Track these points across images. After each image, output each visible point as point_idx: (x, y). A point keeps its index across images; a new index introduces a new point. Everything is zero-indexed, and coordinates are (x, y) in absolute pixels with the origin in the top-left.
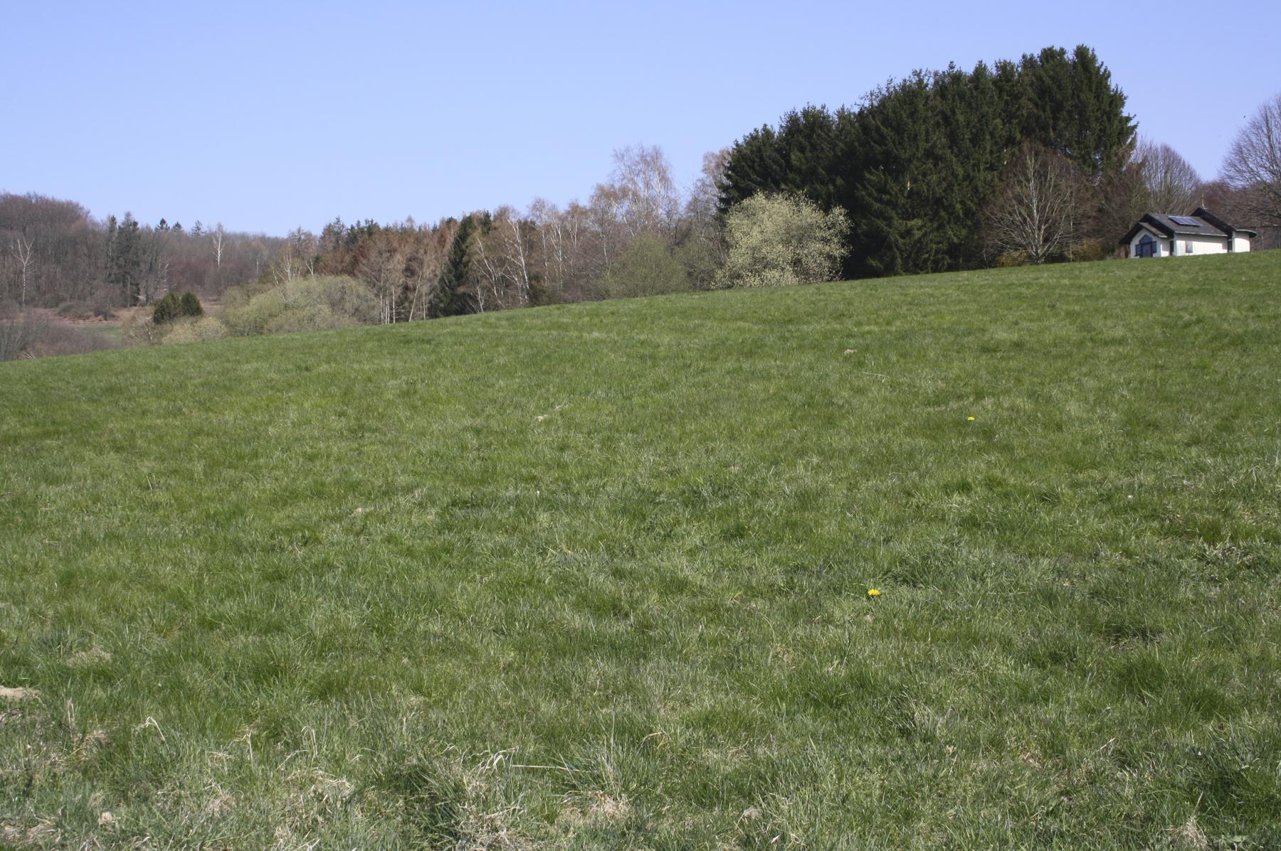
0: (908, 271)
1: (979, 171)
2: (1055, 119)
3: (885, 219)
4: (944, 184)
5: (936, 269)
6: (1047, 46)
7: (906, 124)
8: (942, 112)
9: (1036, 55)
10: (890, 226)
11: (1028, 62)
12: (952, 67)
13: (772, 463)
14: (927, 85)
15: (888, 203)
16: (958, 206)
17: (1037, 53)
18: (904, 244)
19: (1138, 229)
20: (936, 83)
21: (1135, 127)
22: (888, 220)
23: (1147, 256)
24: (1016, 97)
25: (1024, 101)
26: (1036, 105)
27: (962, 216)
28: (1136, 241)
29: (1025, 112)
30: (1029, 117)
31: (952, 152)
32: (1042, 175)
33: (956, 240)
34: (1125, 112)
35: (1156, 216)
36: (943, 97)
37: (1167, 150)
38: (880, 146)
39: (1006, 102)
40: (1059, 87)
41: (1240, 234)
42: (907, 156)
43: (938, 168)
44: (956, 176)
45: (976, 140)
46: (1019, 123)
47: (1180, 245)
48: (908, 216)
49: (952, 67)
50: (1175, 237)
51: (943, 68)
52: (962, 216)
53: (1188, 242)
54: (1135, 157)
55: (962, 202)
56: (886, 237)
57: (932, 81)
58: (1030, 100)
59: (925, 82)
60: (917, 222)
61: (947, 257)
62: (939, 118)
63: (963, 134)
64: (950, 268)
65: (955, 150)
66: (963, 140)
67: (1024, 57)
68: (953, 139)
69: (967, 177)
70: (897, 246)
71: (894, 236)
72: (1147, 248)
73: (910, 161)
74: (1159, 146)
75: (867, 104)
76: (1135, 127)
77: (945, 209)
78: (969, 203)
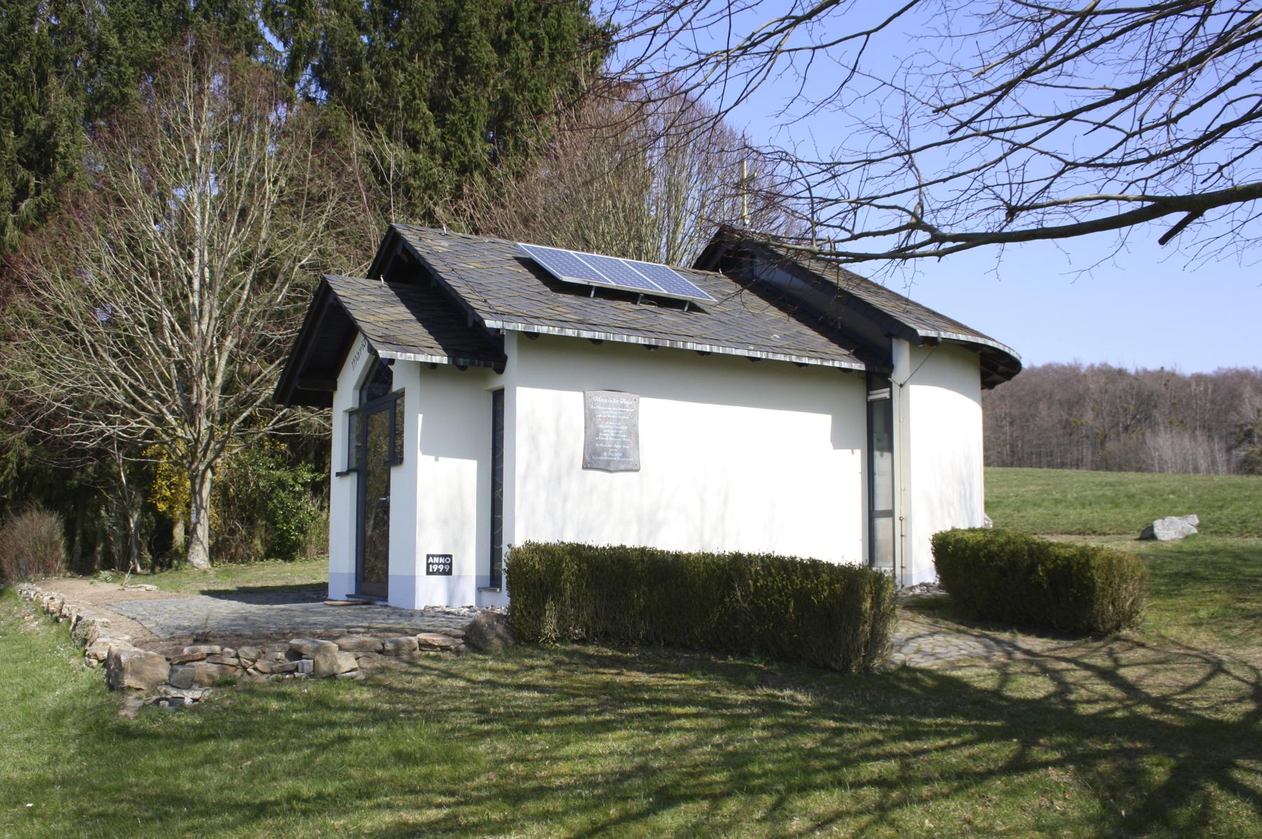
53: (610, 403)
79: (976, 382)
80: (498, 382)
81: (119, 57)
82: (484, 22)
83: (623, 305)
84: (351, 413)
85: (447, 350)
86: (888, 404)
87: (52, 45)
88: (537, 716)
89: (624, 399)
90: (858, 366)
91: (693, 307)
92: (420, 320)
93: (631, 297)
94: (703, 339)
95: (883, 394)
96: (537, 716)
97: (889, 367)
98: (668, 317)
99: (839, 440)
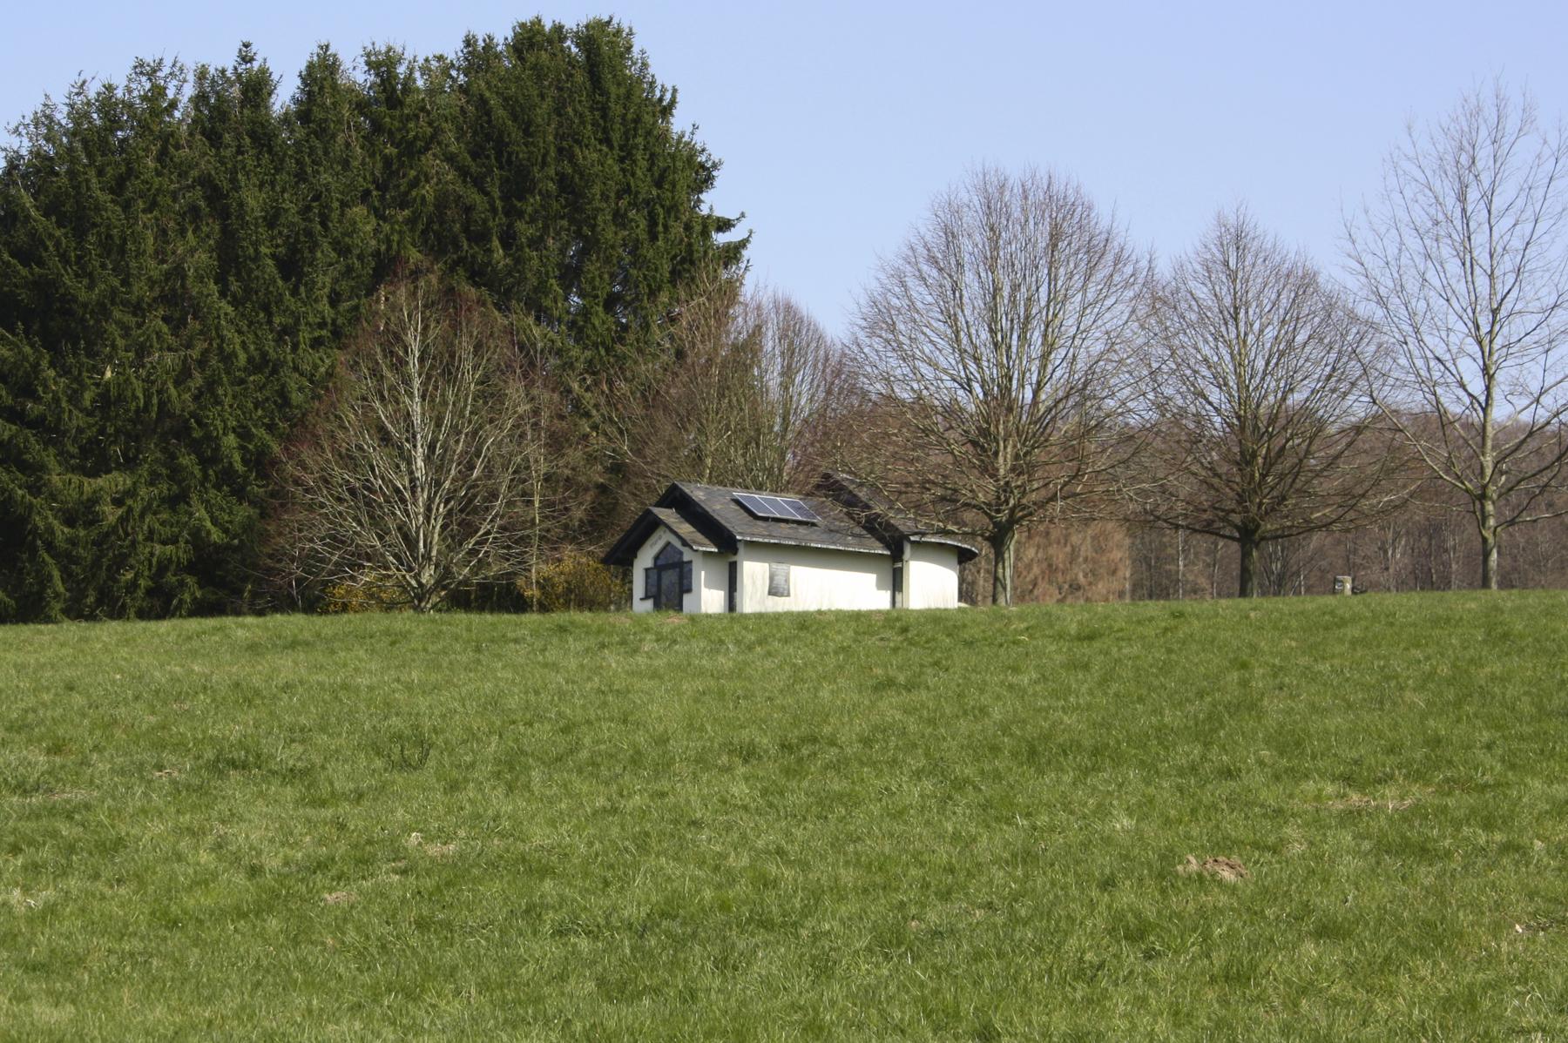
0: (75, 612)
1: (295, 347)
2: (512, 213)
3: (24, 467)
4: (198, 380)
5: (160, 605)
6: (527, 17)
7: (98, 208)
8: (206, 182)
9: (499, 39)
10: (34, 490)
11: (479, 56)
12: (246, 59)
13: (231, 864)
14: (173, 105)
15: (37, 424)
16: (231, 440)
17: (502, 33)
18: (73, 542)
19: (648, 526)
20: (200, 99)
21: (743, 244)
22: (32, 471)
23: (668, 607)
24: (411, 150)
25: (432, 162)
26: (464, 172)
27: (239, 467)
28: (645, 559)
29: (428, 191)
30: (442, 203)
31: (223, 294)
32: (442, 367)
33: (216, 536)
34: (713, 202)
35: (698, 492)
36: (213, 138)
37: (788, 312)
38: (25, 264)
39: (387, 162)
40: (527, 129)
41: (936, 551)
42: (94, 295)
43: (185, 333)
44: (227, 358)
45: (291, 266)
46: (412, 222)
47: (754, 572)
48: (93, 460)
49: (246, 59)
50: (742, 549)
51: (224, 59)
52: (239, 467)
53: (780, 568)
54: (740, 325)
55: (244, 434)
56: (24, 520)
57: (189, 90)
58: (450, 159)
59: (171, 94)
60: (117, 481)
61: (190, 580)
62: (197, 196)
63: (256, 244)
64: (203, 609)
65: (235, 286)
66: (257, 258)
67: (469, 42)
68: (230, 261)
69: (261, 364)
70: (50, 546)
71: (46, 519)
72: (670, 577)
73: (103, 311)
74: (766, 301)
75: (24, 146)
76: (743, 244)
77: (195, 447)
78: (261, 432)
79: (955, 561)
80: (733, 559)
81: (256, 219)
82: (605, 197)
83: (783, 525)
84: (647, 570)
85: (716, 545)
86: (901, 569)
87: (1373, 908)
88: (962, 352)
89: (784, 566)
90: (887, 552)
91: (814, 525)
92: (699, 531)
93: (786, 521)
94: (818, 542)
95: (899, 565)
96: (962, 352)
97: (902, 552)
98: (802, 530)
99: (880, 586)
